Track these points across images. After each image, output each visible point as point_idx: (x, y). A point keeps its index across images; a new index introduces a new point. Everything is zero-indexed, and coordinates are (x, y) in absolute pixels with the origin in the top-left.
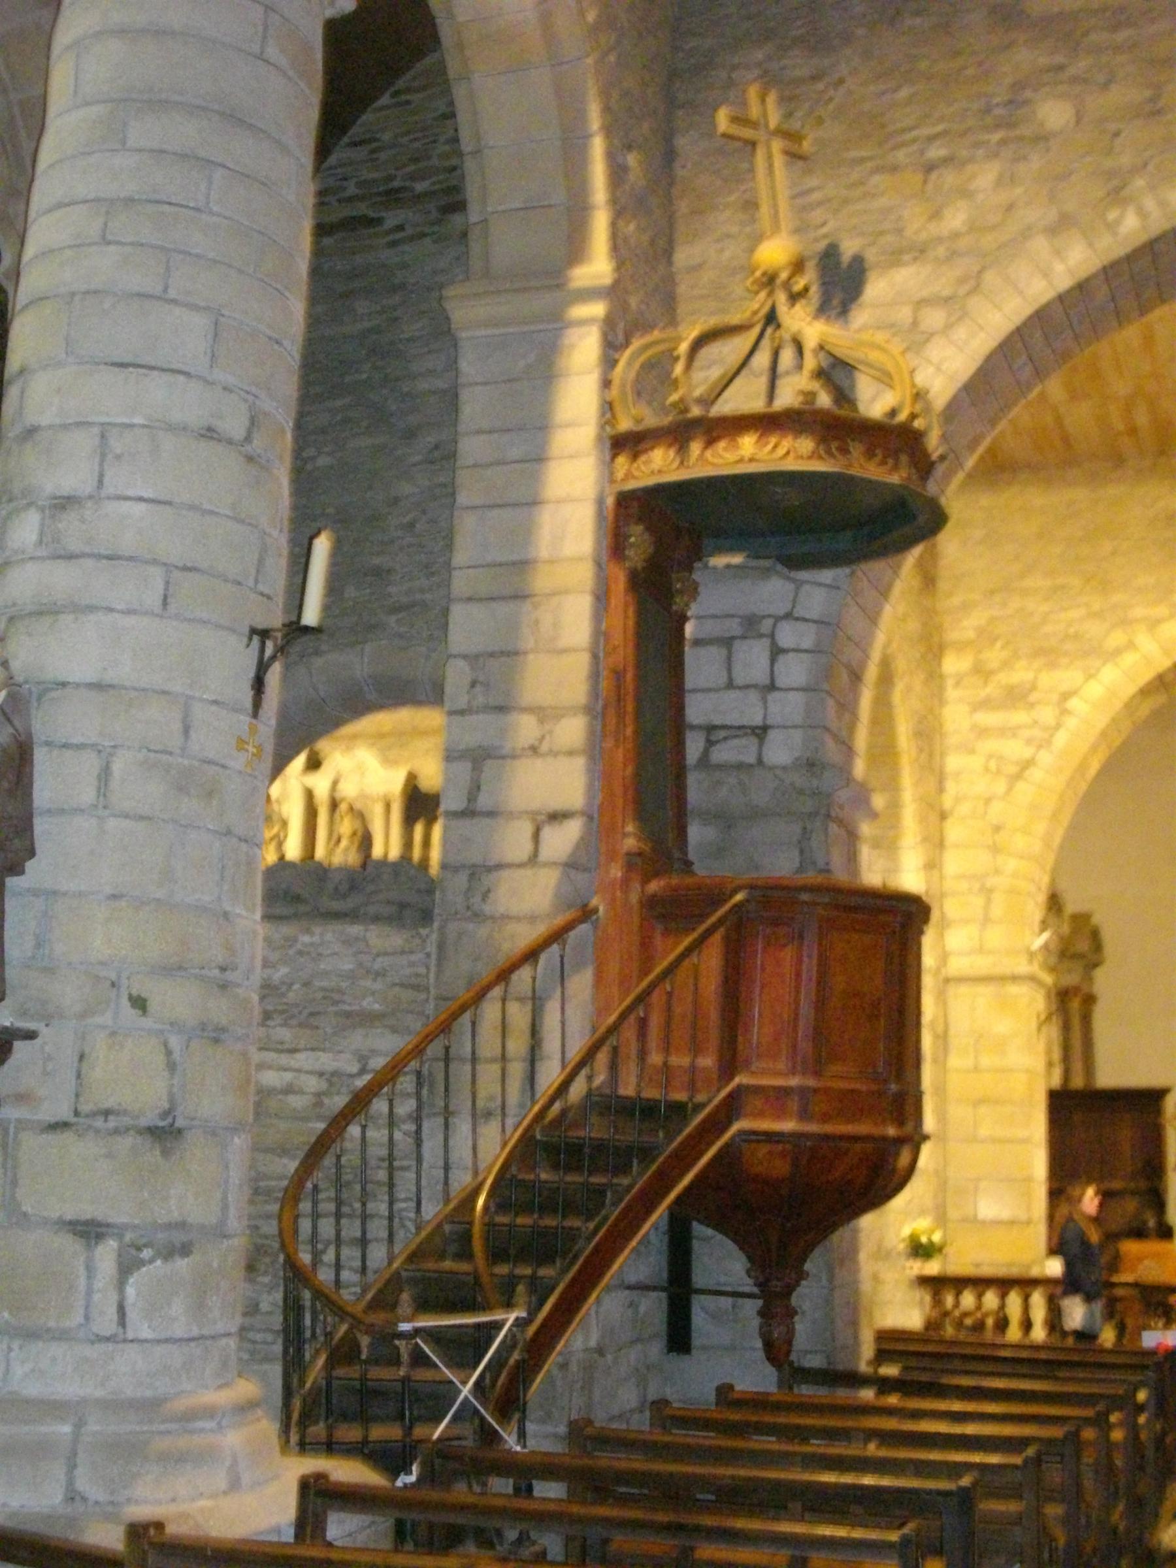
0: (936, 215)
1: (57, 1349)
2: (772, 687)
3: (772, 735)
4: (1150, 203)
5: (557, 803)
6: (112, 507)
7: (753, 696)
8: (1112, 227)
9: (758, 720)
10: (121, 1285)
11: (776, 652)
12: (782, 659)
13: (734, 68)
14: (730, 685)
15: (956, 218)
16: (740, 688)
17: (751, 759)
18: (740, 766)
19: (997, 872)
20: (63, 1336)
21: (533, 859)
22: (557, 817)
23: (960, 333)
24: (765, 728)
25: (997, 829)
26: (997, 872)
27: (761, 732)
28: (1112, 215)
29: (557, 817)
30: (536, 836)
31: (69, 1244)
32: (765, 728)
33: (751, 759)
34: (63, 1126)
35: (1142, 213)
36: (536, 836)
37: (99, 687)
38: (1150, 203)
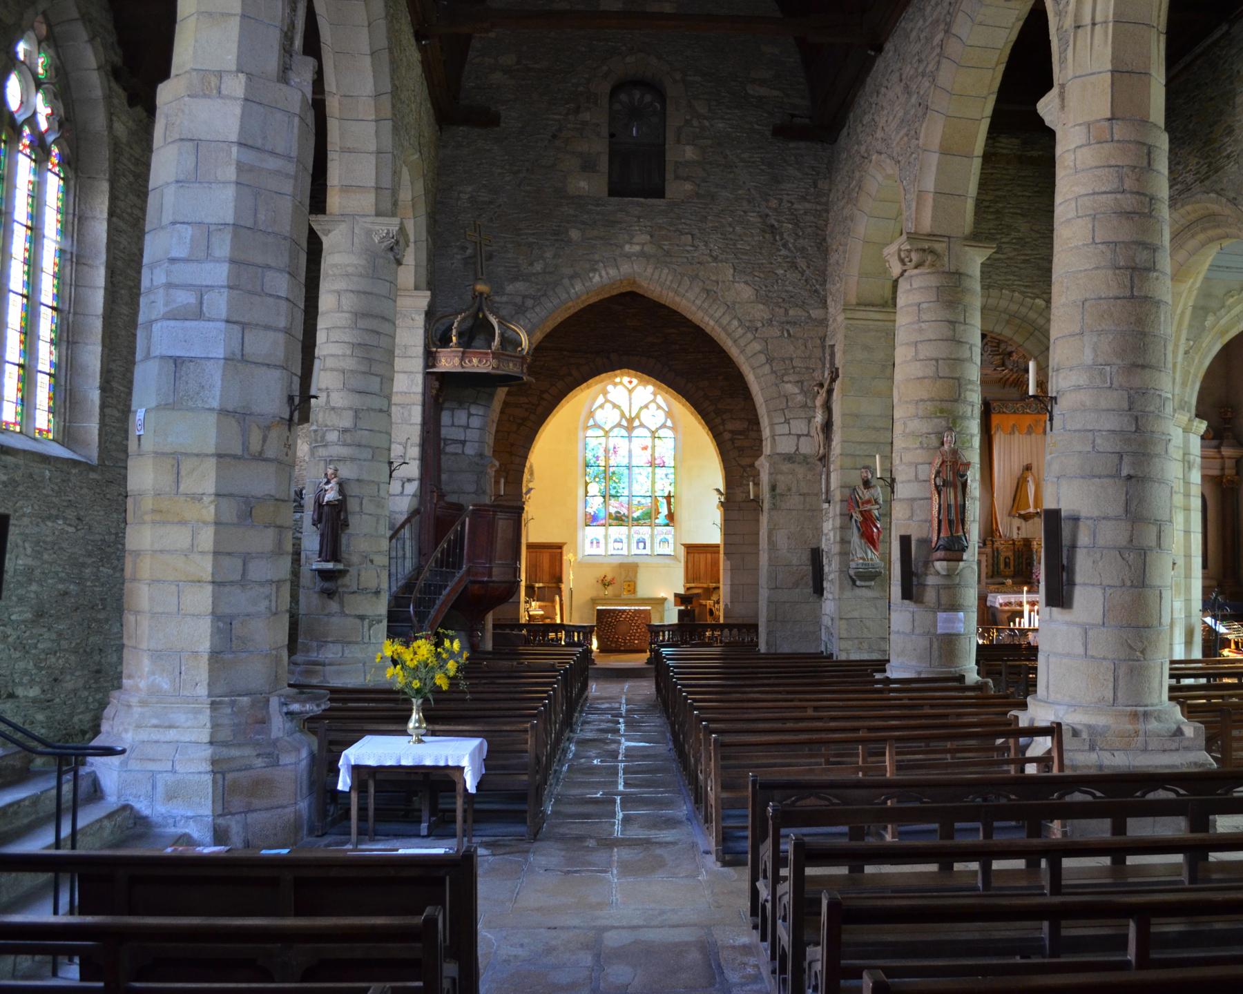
0: (531, 264)
1: (356, 646)
2: (468, 427)
3: (467, 444)
4: (603, 273)
5: (410, 476)
6: (359, 432)
7: (461, 430)
8: (591, 279)
9: (463, 438)
10: (369, 630)
11: (470, 415)
12: (471, 418)
13: (460, 192)
14: (453, 425)
15: (538, 267)
16: (370, 447)
17: (460, 452)
18: (456, 454)
19: (512, 463)
20: (357, 643)
21: (402, 493)
22: (409, 480)
23: (537, 309)
24: (465, 441)
25: (512, 445)
26: (512, 463)
27: (463, 443)
28: (591, 275)
29: (409, 480)
30: (403, 486)
31: (358, 621)
32: (465, 441)
33: (460, 452)
34: (354, 593)
35: (601, 276)
36: (403, 486)
37: (358, 480)
38: (603, 273)
